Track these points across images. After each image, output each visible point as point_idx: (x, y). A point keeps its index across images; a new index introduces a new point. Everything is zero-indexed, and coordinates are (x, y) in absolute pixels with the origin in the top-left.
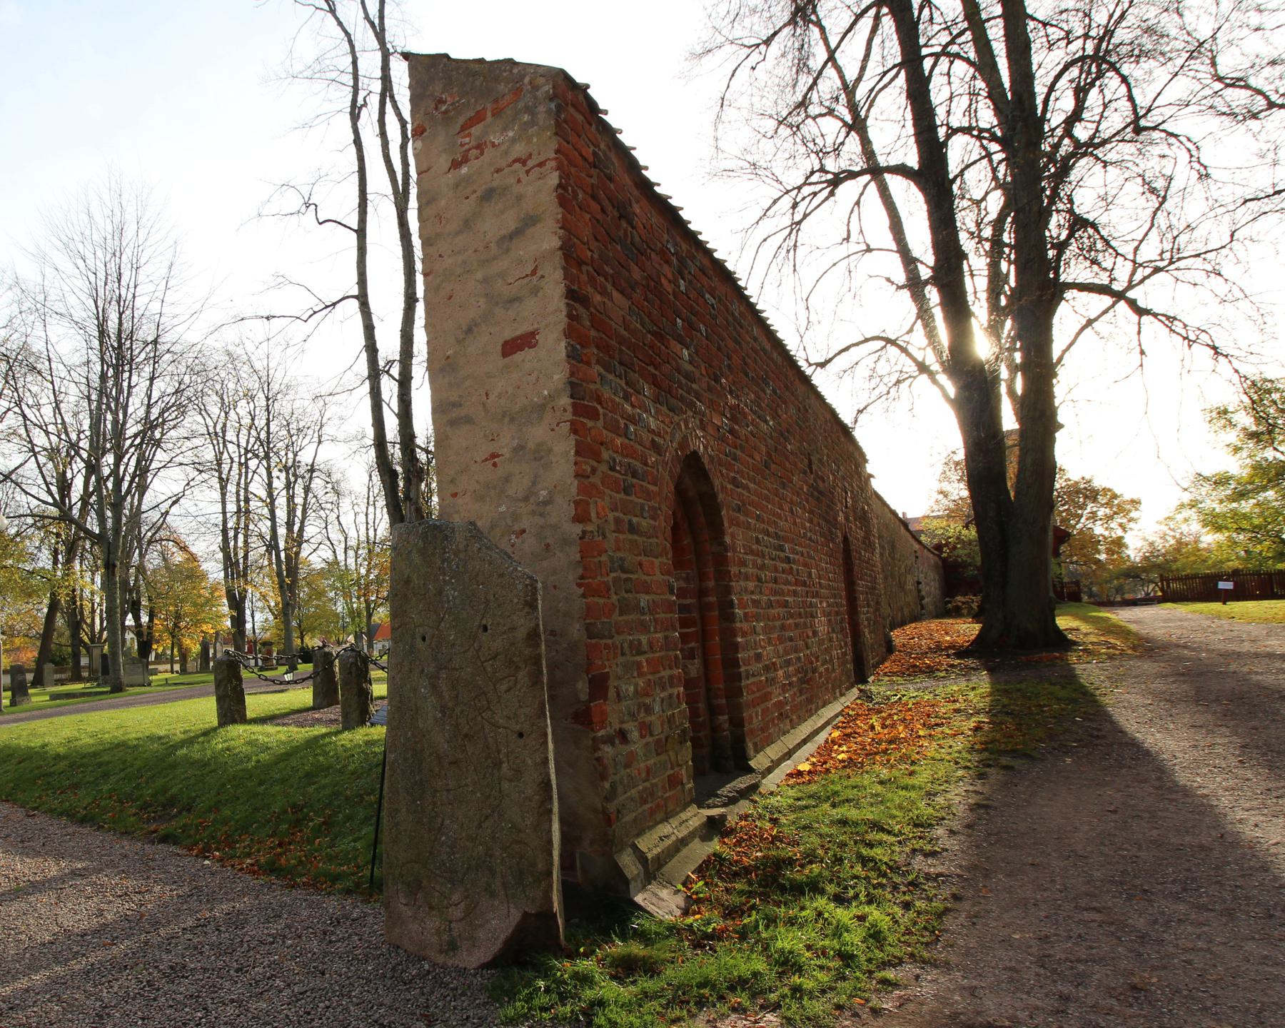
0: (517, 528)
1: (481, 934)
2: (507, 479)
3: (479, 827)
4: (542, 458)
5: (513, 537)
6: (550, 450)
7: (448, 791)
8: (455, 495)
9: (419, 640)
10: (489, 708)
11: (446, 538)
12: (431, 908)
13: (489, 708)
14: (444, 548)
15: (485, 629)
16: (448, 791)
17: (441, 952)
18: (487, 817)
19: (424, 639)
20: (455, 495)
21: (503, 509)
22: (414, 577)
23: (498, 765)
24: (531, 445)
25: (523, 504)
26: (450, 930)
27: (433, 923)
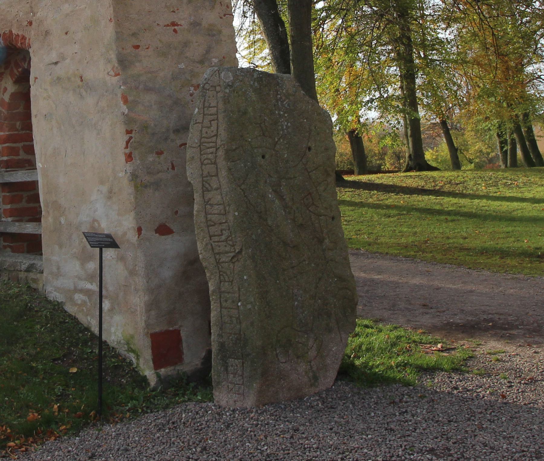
0: (194, 82)
1: (329, 361)
2: (186, 44)
3: (316, 287)
4: (214, 35)
5: (192, 89)
6: (220, 32)
7: (293, 267)
8: (137, 47)
9: (259, 158)
10: (313, 204)
11: (278, 84)
12: (298, 357)
13: (313, 204)
14: (277, 91)
15: (310, 149)
16: (293, 267)
17: (311, 385)
18: (320, 279)
19: (263, 157)
20: (137, 47)
21: (182, 66)
22: (250, 110)
23: (321, 241)
24: (204, 24)
25: (199, 65)
26: (311, 367)
27: (302, 367)
